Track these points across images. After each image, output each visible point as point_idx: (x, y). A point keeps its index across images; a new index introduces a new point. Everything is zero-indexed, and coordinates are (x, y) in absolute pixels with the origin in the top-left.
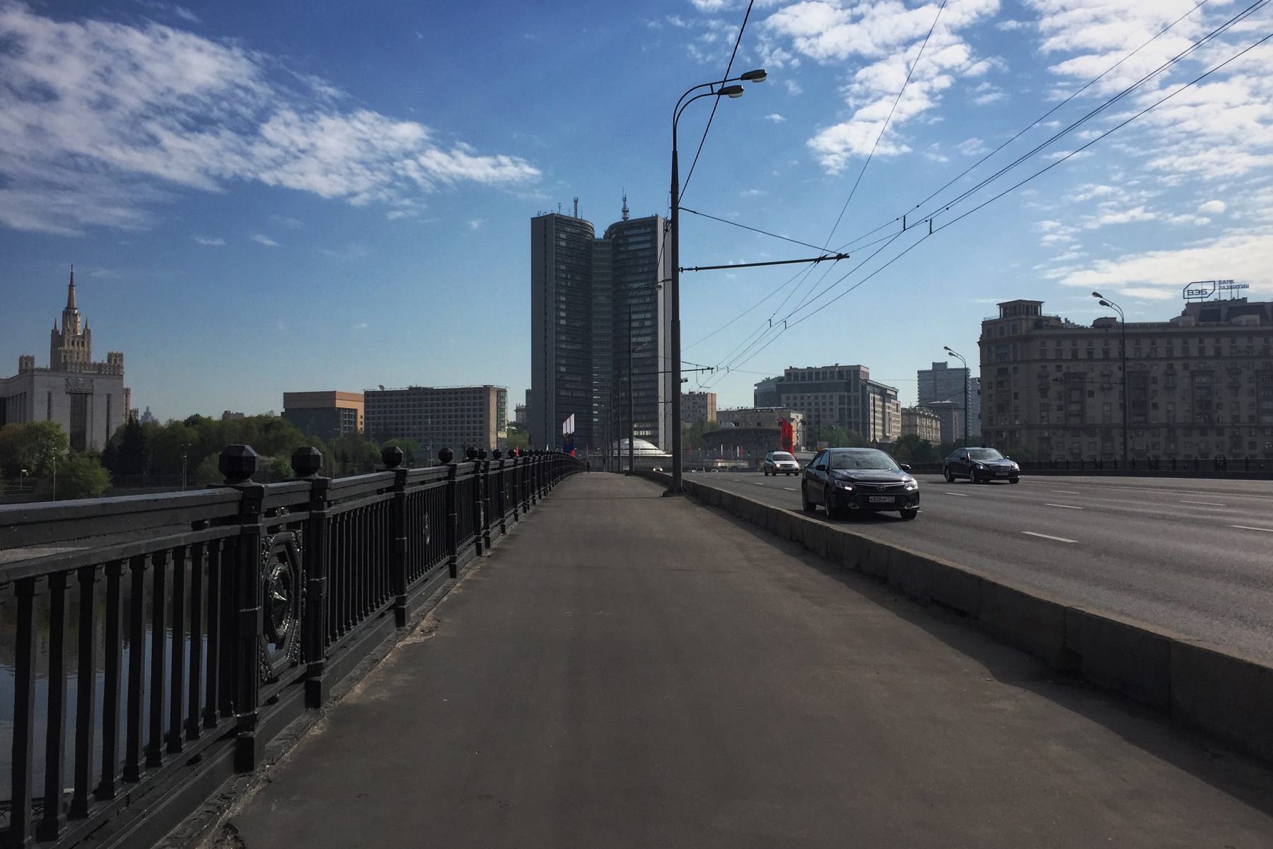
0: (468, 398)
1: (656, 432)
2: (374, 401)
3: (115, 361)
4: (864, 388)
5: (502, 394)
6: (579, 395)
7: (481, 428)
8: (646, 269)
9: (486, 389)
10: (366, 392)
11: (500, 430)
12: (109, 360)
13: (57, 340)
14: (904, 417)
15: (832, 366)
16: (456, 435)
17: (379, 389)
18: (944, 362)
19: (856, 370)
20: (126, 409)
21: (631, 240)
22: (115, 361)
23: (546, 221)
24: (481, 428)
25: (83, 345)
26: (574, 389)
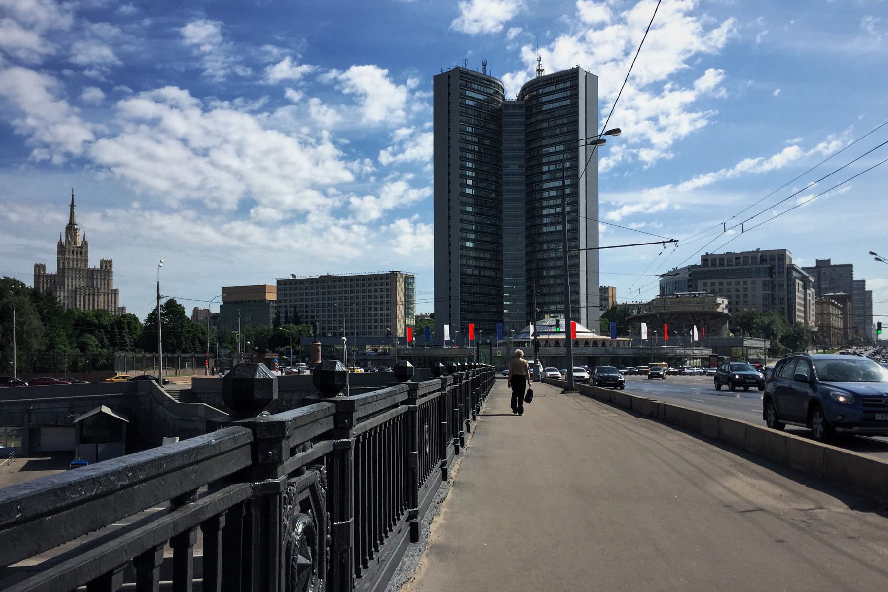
0: (375, 285)
1: (577, 315)
2: (285, 290)
3: (107, 265)
4: (789, 273)
5: (410, 281)
6: (488, 273)
7: (388, 315)
8: (565, 129)
9: (394, 274)
10: (278, 281)
11: (408, 317)
12: (101, 266)
13: (61, 249)
14: (818, 306)
15: (753, 251)
16: (364, 322)
17: (291, 278)
18: (827, 259)
19: (781, 255)
20: (115, 307)
21: (544, 99)
22: (107, 265)
23: (449, 77)
24: (388, 315)
25: (81, 254)
26: (483, 267)
